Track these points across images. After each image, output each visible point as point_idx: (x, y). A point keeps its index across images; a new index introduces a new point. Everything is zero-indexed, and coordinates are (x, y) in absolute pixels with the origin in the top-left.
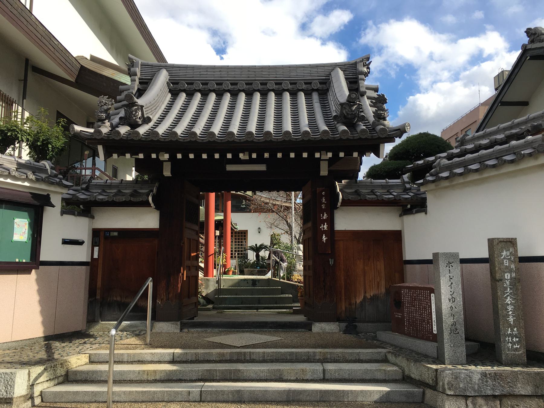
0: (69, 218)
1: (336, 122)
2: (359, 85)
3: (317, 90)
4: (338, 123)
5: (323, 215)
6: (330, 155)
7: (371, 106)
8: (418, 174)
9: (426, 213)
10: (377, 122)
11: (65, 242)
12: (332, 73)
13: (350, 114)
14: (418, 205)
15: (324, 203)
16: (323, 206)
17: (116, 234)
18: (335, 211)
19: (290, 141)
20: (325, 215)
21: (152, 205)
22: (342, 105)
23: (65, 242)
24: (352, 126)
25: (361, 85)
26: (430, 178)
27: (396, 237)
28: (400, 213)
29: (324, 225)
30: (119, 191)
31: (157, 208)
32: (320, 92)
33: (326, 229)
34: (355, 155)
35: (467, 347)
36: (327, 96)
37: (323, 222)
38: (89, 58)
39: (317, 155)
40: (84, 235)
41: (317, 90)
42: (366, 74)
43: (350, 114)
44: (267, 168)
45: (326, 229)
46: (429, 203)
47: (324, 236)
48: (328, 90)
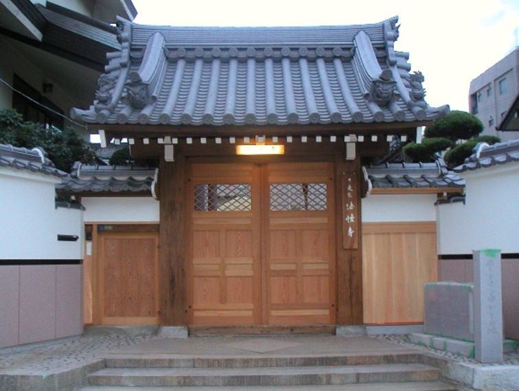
0: (62, 210)
1: (367, 101)
2: (387, 52)
3: (340, 57)
4: (370, 101)
5: (349, 206)
6: (175, 141)
7: (406, 86)
8: (458, 158)
9: (464, 203)
10: (413, 103)
11: (61, 238)
12: (356, 37)
13: (381, 92)
14: (455, 195)
15: (350, 191)
16: (349, 195)
17: (110, 228)
18: (363, 201)
19: (340, 124)
20: (352, 205)
21: (154, 195)
22: (374, 82)
23: (61, 238)
24: (386, 104)
25: (390, 52)
26: (469, 165)
27: (430, 230)
28: (436, 201)
29: (350, 216)
30: (95, 179)
31: (158, 198)
32: (343, 59)
33: (352, 221)
34: (232, 140)
35: (504, 344)
36: (351, 64)
37: (349, 213)
38: (44, 4)
39: (160, 141)
40: (78, 231)
41: (340, 57)
42: (395, 39)
43: (381, 92)
44: (364, 140)
45: (352, 221)
46: (467, 191)
47: (350, 229)
48: (352, 57)
